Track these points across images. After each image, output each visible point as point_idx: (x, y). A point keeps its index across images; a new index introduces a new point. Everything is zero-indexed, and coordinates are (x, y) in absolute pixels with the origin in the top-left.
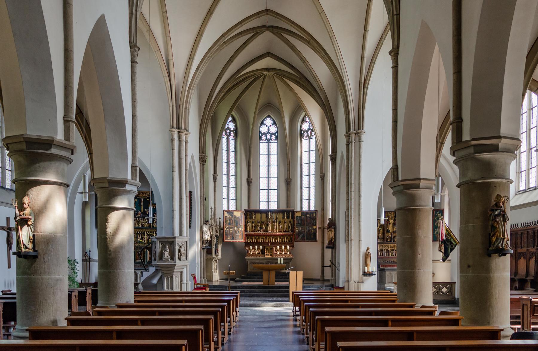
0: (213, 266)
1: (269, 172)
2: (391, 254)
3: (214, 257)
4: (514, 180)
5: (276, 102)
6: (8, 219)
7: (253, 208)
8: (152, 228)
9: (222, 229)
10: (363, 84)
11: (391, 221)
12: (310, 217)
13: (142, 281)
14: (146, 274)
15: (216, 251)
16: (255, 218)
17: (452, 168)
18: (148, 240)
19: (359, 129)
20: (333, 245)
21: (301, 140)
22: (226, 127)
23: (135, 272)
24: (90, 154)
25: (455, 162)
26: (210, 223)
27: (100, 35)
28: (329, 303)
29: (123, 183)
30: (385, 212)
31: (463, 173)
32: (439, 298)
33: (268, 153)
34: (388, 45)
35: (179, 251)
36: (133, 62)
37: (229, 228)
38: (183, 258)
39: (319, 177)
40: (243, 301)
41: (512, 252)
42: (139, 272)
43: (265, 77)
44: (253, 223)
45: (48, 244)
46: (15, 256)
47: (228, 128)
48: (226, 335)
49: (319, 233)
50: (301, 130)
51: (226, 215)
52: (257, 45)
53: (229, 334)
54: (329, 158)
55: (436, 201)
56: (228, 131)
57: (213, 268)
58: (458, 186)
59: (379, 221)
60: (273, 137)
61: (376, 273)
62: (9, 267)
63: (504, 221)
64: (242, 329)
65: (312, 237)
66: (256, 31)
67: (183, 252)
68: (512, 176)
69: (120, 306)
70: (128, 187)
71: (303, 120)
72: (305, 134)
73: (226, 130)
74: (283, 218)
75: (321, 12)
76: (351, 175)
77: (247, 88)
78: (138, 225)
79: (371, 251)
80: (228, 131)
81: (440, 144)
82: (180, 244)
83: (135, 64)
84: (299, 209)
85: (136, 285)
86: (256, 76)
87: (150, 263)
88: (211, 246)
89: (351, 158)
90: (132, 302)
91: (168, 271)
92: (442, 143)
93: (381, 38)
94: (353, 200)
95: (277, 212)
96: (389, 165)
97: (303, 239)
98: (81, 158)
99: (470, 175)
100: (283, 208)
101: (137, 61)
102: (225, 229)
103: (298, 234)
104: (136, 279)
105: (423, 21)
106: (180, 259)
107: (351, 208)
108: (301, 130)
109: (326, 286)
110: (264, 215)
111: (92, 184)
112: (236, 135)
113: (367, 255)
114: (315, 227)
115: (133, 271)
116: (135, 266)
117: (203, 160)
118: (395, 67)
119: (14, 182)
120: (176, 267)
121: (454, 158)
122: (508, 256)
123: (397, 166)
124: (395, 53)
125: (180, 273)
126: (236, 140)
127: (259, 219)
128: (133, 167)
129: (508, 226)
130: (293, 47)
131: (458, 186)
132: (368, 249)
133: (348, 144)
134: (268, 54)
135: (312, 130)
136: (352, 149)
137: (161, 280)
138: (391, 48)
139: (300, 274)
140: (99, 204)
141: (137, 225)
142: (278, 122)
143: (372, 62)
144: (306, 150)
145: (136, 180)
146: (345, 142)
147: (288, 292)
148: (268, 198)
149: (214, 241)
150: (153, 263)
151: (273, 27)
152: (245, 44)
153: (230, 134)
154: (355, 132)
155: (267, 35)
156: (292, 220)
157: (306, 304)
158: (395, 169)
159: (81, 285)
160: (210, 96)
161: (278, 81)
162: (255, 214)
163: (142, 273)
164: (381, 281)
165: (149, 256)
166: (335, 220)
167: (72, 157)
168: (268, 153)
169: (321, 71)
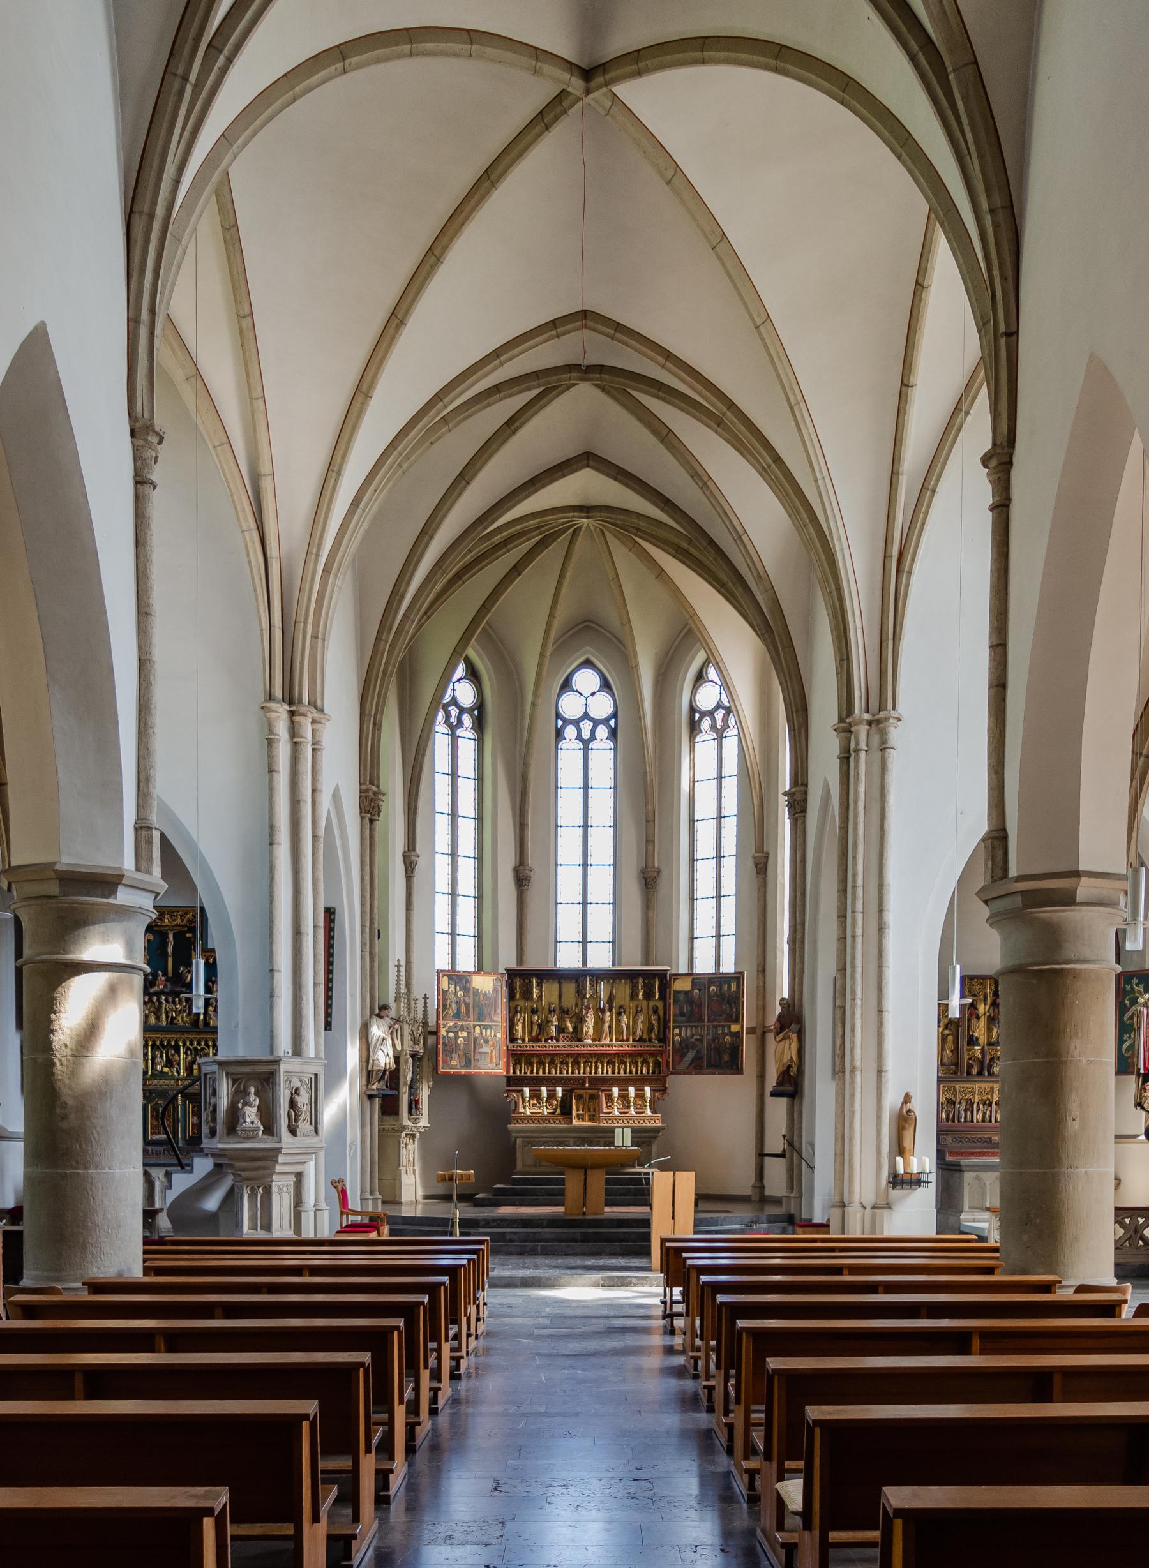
0: (403, 1152)
2: (980, 1116)
3: (407, 1122)
5: (612, 618)
7: (533, 962)
8: (203, 1030)
9: (431, 1033)
11: (982, 1009)
12: (720, 996)
13: (169, 1201)
14: (182, 1182)
18: (189, 1068)
19: (882, 707)
20: (792, 1085)
21: (692, 749)
22: (447, 698)
23: (146, 1174)
30: (963, 979)
33: (585, 784)
35: (292, 1104)
36: (141, 481)
37: (456, 1030)
38: (304, 1126)
39: (750, 863)
40: (500, 1269)
42: (158, 1174)
44: (534, 1011)
47: (454, 702)
50: (693, 710)
51: (445, 986)
53: (455, 1376)
54: (783, 801)
56: (454, 711)
59: (943, 1009)
64: (495, 1360)
65: (725, 1060)
66: (549, 383)
69: (97, 1287)
70: (123, 897)
71: (700, 678)
72: (706, 724)
73: (445, 707)
74: (633, 996)
75: (761, 323)
76: (854, 858)
77: (516, 570)
78: (157, 1018)
79: (916, 1105)
80: (454, 711)
82: (296, 1083)
84: (683, 969)
85: (149, 1215)
86: (548, 531)
88: (397, 1088)
91: (253, 1170)
93: (957, 409)
97: (697, 1067)
100: (633, 962)
102: (443, 1032)
103: (682, 1049)
105: (1092, 358)
108: (693, 710)
110: (570, 988)
112: (479, 725)
113: (904, 1120)
114: (735, 1028)
115: (140, 1170)
116: (145, 1152)
120: (281, 1159)
123: (1004, 829)
124: (1001, 460)
125: (293, 1178)
128: (142, 827)
130: (666, 436)
132: (907, 1099)
133: (845, 758)
134: (588, 459)
135: (728, 711)
136: (857, 775)
141: (152, 1020)
143: (927, 488)
144: (709, 773)
145: (149, 872)
146: (837, 752)
147: (647, 1237)
148: (585, 929)
150: (207, 1143)
151: (601, 369)
152: (512, 425)
153: (460, 723)
154: (868, 717)
156: (660, 1005)
160: (396, 594)
161: (619, 551)
162: (539, 985)
163: (168, 1175)
164: (948, 1202)
165: (192, 1120)
168: (585, 784)
169: (758, 518)
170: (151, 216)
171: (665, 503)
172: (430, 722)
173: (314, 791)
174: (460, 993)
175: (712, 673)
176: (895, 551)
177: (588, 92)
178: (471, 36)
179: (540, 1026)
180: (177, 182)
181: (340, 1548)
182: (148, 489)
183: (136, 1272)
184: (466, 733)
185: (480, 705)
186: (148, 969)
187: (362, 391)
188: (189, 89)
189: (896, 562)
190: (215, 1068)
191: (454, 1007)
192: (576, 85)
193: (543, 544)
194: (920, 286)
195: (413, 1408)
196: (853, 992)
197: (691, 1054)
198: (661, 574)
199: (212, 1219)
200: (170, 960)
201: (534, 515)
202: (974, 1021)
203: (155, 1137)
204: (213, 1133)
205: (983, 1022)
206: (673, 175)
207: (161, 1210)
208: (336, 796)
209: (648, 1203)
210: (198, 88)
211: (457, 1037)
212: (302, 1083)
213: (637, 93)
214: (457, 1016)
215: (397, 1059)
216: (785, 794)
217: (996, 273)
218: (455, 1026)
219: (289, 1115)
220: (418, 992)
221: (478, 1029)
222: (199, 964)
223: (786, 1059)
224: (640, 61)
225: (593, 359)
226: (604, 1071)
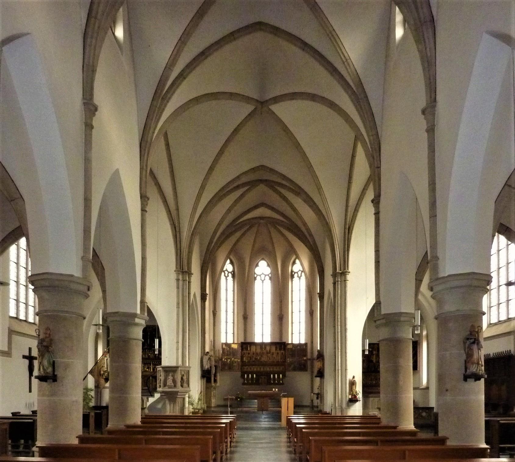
1: (264, 305)
3: (213, 384)
4: (486, 312)
6: (30, 349)
7: (249, 340)
8: (158, 359)
11: (374, 352)
12: (301, 349)
13: (148, 405)
14: (151, 400)
16: (250, 349)
18: (154, 369)
19: (344, 269)
20: (321, 374)
21: (292, 281)
22: (224, 269)
24: (104, 291)
26: (210, 354)
28: (317, 426)
29: (135, 315)
32: (421, 422)
34: (370, 195)
35: (182, 379)
36: (143, 210)
37: (227, 359)
38: (185, 385)
41: (486, 376)
42: (145, 398)
45: (66, 369)
46: (37, 380)
47: (226, 270)
48: (224, 454)
50: (292, 271)
52: (253, 197)
53: (231, 447)
54: (318, 296)
55: (416, 332)
58: (436, 318)
59: (363, 351)
60: (267, 278)
62: (30, 391)
63: (479, 349)
64: (238, 449)
65: (302, 367)
66: (252, 184)
68: (485, 309)
70: (137, 320)
71: (294, 263)
72: (296, 275)
73: (224, 272)
74: (276, 350)
75: (310, 167)
79: (356, 379)
80: (226, 272)
81: (419, 281)
82: (183, 373)
83: (144, 212)
84: (290, 342)
85: (143, 409)
86: (252, 223)
87: (155, 390)
90: (139, 423)
91: (171, 396)
92: (421, 281)
94: (339, 333)
95: (272, 344)
97: (295, 369)
98: (96, 293)
100: (278, 341)
101: (147, 209)
103: (290, 365)
104: (143, 404)
106: (182, 386)
108: (292, 271)
109: (315, 412)
110: (259, 347)
112: (233, 276)
113: (353, 383)
114: (305, 358)
117: (203, 297)
119: (37, 314)
120: (179, 394)
122: (483, 380)
124: (376, 202)
126: (234, 280)
127: (254, 350)
129: (483, 352)
131: (436, 318)
132: (354, 377)
133: (334, 284)
135: (302, 272)
136: (338, 288)
139: (291, 400)
140: (111, 335)
141: (144, 356)
142: (273, 264)
143: (356, 210)
144: (298, 289)
145: (144, 314)
146: (332, 282)
148: (263, 332)
150: (158, 389)
151: (266, 180)
153: (228, 276)
154: (341, 274)
155: (262, 188)
159: (95, 408)
161: (272, 230)
162: (250, 347)
169: (308, 215)
175: (297, 261)
176: (347, 227)
178: (231, 94)
181: (215, 460)
183: (139, 423)
184: (230, 278)
185: (234, 271)
187: (203, 188)
189: (348, 230)
190: (161, 369)
193: (251, 227)
194: (353, 156)
195: (222, 453)
197: (292, 366)
198: (283, 235)
199: (160, 410)
208: (195, 295)
209: (281, 407)
213: (276, 108)
214: (227, 355)
222: (157, 341)
224: (276, 100)
225: (265, 178)
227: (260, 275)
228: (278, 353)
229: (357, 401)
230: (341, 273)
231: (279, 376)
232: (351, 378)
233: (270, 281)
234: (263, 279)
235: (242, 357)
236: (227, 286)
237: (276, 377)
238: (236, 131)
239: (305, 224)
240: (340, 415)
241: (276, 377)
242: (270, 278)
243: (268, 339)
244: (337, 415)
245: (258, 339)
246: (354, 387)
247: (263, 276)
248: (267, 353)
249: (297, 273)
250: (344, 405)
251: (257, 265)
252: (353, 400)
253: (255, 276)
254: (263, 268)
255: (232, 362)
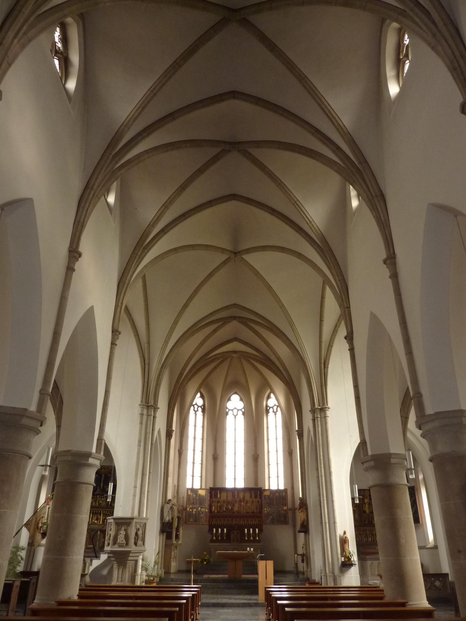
0: (173, 553)
1: (236, 446)
2: (370, 539)
3: (174, 542)
5: (243, 381)
7: (219, 486)
8: (110, 508)
9: (184, 509)
10: (323, 365)
11: (366, 501)
12: (279, 497)
14: (96, 563)
15: (177, 537)
17: (420, 442)
18: (103, 521)
19: (324, 404)
20: (305, 528)
21: (267, 416)
22: (194, 403)
23: (84, 560)
24: (59, 427)
25: (423, 436)
27: (88, 319)
30: (359, 490)
31: (433, 445)
33: (235, 427)
34: (343, 332)
35: (137, 534)
36: (113, 344)
37: (192, 508)
38: (140, 542)
40: (205, 599)
42: (88, 560)
43: (232, 358)
44: (218, 502)
49: (290, 514)
50: (267, 406)
51: (189, 493)
55: (411, 477)
56: (196, 407)
57: (173, 556)
60: (240, 413)
61: (357, 563)
66: (225, 321)
67: (141, 536)
69: (61, 603)
70: (91, 461)
71: (269, 397)
72: (271, 410)
73: (193, 406)
74: (251, 497)
76: (319, 450)
77: (215, 368)
78: (95, 503)
80: (196, 407)
82: (138, 526)
84: (267, 488)
85: (83, 576)
88: (172, 529)
89: (318, 433)
91: (121, 558)
93: (336, 326)
95: (245, 490)
96: (357, 440)
97: (273, 522)
98: (49, 428)
99: (442, 448)
100: (252, 486)
101: (117, 343)
102: (188, 509)
105: (371, 312)
107: (322, 486)
111: (55, 457)
112: (203, 411)
113: (344, 541)
114: (285, 508)
115: (82, 557)
116: (85, 552)
117: (169, 435)
118: (352, 350)
120: (131, 555)
121: (421, 432)
123: (365, 440)
124: (350, 338)
125: (134, 562)
126: (204, 415)
127: (225, 498)
128: (100, 439)
132: (345, 533)
134: (235, 339)
135: (278, 406)
136: (318, 425)
137: (111, 572)
138: (346, 334)
141: (94, 504)
142: (245, 398)
144: (274, 425)
145: (100, 453)
146: (311, 418)
147: (257, 587)
148: (235, 477)
149: (175, 524)
152: (215, 331)
153: (198, 410)
154: (320, 410)
155: (235, 323)
156: (260, 500)
157: (279, 602)
158: (363, 445)
160: (181, 374)
161: (244, 363)
162: (220, 493)
163: (91, 561)
164: (363, 573)
165: (102, 540)
166: (306, 500)
167: (40, 428)
168: (235, 427)
169: (282, 350)
170: (125, 283)
171: (257, 350)
172: (189, 409)
173: (153, 430)
174: (194, 496)
176: (323, 362)
177: (235, 257)
179: (220, 507)
180: (132, 276)
182: (114, 346)
185: (204, 405)
186: (95, 485)
187: (176, 323)
188: (138, 257)
190: (112, 521)
191: (192, 500)
192: (233, 256)
196: (323, 495)
197: (271, 517)
200: (102, 484)
201: (220, 353)
202: (364, 505)
203: (89, 546)
204: (109, 545)
205: (367, 506)
206: (257, 273)
207: (87, 574)
209: (257, 574)
210: (140, 256)
211: (193, 511)
212: (141, 526)
215: (172, 518)
216: (297, 431)
217: (342, 294)
218: (192, 507)
219: (135, 538)
220: (181, 495)
221: (200, 508)
222: (111, 485)
223: (302, 519)
224: (248, 251)
226: (242, 522)
227: (232, 410)
228: (253, 502)
229: (351, 565)
230: (320, 409)
231: (254, 531)
232: (342, 534)
233: (243, 416)
234: (235, 414)
235: (210, 506)
236: (196, 421)
237: (251, 532)
238: (211, 275)
239: (278, 358)
240: (332, 585)
241: (251, 532)
242: (244, 414)
243: (241, 484)
244: (329, 586)
245: (229, 484)
246: (346, 546)
247: (235, 411)
248: (240, 501)
249: (272, 408)
250: (337, 571)
251: (229, 399)
252: (347, 565)
253: (227, 410)
254: (235, 403)
255: (199, 513)
